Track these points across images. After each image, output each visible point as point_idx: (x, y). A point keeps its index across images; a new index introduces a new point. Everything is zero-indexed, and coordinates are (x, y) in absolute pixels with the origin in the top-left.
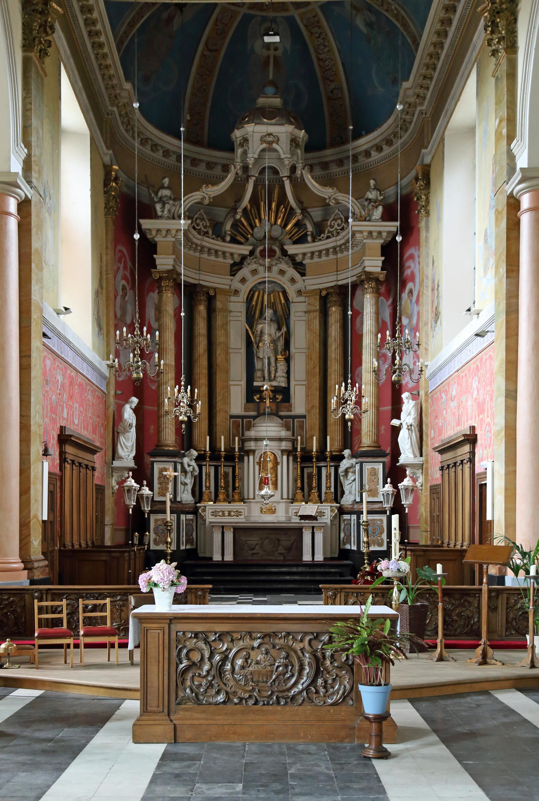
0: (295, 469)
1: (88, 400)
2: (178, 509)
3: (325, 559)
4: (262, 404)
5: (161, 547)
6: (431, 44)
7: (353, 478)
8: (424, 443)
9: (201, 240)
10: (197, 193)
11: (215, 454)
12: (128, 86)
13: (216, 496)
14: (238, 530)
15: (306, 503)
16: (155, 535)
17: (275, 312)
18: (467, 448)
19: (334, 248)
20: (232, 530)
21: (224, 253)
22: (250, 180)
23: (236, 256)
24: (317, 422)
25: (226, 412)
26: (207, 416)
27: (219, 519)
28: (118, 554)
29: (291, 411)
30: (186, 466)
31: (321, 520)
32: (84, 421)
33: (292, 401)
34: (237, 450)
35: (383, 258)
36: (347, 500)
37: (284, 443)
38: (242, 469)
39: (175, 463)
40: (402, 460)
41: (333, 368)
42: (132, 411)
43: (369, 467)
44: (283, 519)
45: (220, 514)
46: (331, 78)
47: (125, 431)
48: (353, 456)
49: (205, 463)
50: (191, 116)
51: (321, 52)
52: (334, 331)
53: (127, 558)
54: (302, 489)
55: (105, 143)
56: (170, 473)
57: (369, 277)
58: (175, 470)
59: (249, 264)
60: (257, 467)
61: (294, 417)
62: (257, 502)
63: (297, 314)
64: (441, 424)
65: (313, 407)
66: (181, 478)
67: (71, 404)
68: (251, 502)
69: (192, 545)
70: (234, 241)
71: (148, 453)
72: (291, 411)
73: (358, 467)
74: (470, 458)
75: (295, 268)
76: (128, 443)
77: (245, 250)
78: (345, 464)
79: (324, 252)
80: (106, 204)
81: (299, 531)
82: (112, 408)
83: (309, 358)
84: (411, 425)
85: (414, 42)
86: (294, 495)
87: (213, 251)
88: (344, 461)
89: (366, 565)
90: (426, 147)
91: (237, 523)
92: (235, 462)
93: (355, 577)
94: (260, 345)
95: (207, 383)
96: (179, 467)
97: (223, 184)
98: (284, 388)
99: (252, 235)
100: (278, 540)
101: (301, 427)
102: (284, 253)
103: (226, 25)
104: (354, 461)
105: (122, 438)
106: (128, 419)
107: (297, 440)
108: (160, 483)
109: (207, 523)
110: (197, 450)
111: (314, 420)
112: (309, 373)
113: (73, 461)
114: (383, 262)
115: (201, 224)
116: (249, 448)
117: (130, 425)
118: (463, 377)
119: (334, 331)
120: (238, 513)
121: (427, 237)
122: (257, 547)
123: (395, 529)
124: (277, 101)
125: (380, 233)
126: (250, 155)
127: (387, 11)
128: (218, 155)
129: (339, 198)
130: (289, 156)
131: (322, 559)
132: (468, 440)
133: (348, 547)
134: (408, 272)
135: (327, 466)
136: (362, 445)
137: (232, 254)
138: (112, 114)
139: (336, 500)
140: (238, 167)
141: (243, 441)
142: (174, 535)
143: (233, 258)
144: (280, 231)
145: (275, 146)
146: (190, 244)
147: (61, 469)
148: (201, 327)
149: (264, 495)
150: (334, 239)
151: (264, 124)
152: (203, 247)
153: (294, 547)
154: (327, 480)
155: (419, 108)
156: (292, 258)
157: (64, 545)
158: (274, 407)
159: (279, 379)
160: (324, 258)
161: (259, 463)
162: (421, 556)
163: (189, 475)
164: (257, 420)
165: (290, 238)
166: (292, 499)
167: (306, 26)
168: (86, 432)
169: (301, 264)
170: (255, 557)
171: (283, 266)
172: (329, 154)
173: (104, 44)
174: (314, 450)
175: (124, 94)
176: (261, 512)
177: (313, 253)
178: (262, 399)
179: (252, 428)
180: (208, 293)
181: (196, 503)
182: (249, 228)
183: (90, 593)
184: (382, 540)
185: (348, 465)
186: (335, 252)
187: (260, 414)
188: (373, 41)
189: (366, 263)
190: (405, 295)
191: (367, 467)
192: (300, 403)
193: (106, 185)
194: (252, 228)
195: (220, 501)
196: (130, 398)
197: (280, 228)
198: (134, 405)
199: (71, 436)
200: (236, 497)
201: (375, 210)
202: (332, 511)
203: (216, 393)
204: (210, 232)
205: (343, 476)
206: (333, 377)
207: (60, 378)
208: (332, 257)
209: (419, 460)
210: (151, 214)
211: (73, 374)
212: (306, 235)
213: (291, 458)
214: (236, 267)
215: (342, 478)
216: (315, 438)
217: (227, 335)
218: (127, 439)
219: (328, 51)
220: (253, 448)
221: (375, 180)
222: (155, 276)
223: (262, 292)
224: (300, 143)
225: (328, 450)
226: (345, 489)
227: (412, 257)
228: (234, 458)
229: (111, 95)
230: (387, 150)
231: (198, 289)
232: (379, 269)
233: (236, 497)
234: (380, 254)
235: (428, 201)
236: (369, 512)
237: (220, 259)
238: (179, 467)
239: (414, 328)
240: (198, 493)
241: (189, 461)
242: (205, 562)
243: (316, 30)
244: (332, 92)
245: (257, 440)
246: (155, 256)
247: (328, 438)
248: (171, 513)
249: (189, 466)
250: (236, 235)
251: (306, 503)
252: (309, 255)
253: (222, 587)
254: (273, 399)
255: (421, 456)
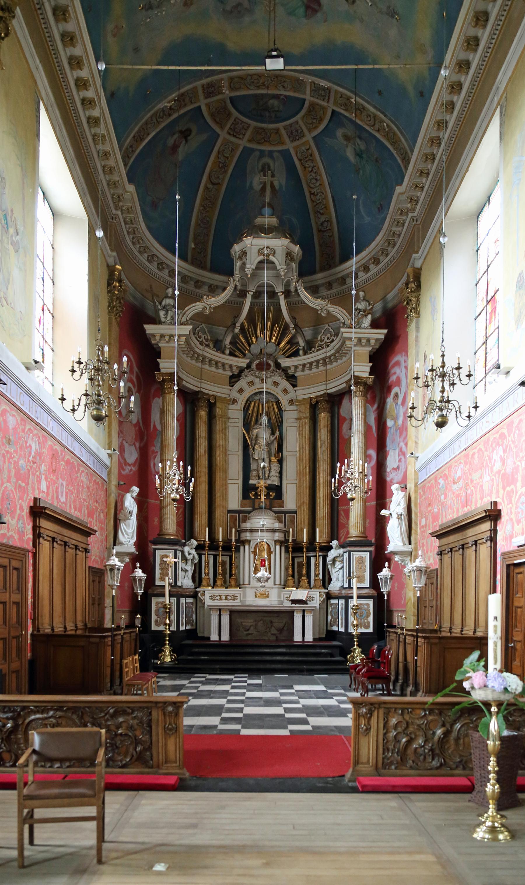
0: (287, 558)
1: (82, 481)
2: (177, 592)
3: (315, 639)
4: (257, 500)
5: (162, 628)
6: (435, 123)
7: (340, 566)
8: (413, 532)
9: (202, 350)
10: (198, 303)
11: (213, 545)
12: (131, 188)
13: (215, 581)
14: (234, 613)
15: (297, 589)
16: (156, 617)
17: (269, 420)
18: (486, 526)
19: (324, 359)
20: (228, 613)
21: (224, 365)
22: (248, 295)
23: (234, 368)
24: (307, 517)
25: (224, 507)
26: (207, 511)
27: (217, 603)
28: (97, 640)
29: (283, 507)
30: (187, 554)
31: (310, 604)
32: (74, 501)
33: (284, 498)
34: (233, 541)
35: (371, 364)
36: (335, 586)
37: (277, 534)
38: (238, 558)
39: (176, 550)
40: (390, 548)
41: (322, 468)
42: (132, 500)
43: (357, 556)
44: (275, 603)
45: (218, 598)
46: (322, 211)
47: (126, 519)
48: (342, 546)
49: (204, 552)
50: (195, 244)
51: (312, 186)
52: (323, 436)
53: (110, 643)
54: (293, 576)
55: (110, 245)
56: (171, 559)
57: (358, 381)
58: (176, 557)
59: (246, 376)
60: (252, 556)
61: (285, 513)
62: (252, 588)
63: (289, 421)
64: (436, 510)
65: (303, 503)
66: (181, 565)
67: (54, 478)
68: (246, 587)
69: (192, 625)
70: (232, 354)
71: (150, 541)
72: (283, 507)
73: (346, 556)
74: (491, 537)
75: (288, 380)
76: (129, 529)
77: (243, 362)
78: (332, 554)
79: (314, 364)
80: (109, 303)
81: (291, 614)
82: (113, 498)
83: (300, 459)
84: (401, 515)
85: (403, 159)
86: (286, 581)
87: (214, 363)
88: (332, 551)
89: (355, 647)
90: (417, 252)
91: (233, 606)
92: (231, 551)
93: (345, 657)
94: (256, 447)
95: (207, 481)
96: (179, 554)
97: (223, 295)
98: (277, 486)
99: (249, 351)
100: (271, 622)
101: (292, 521)
102: (278, 365)
103: (227, 158)
104: (341, 551)
105: (123, 526)
106: (128, 507)
107: (288, 532)
108: (161, 569)
109: (206, 606)
110: (197, 541)
111: (303, 516)
112: (299, 473)
113: (53, 540)
114: (371, 368)
115: (203, 337)
116: (245, 539)
117: (131, 513)
118: (474, 454)
119: (323, 436)
120: (234, 598)
121: (417, 337)
122: (252, 628)
123: (496, 618)
124: (274, 221)
125: (368, 340)
126: (248, 266)
127: (378, 131)
128: (218, 278)
129: (330, 309)
130: (285, 267)
131: (311, 640)
132: (489, 516)
133: (335, 628)
134: (393, 378)
135: (316, 556)
136: (350, 536)
137: (231, 366)
138: (116, 218)
139: (324, 586)
140: (237, 279)
141: (239, 532)
142: (174, 617)
143: (231, 370)
144: (275, 348)
145: (272, 258)
146: (192, 352)
147: (34, 545)
148: (202, 431)
149: (261, 578)
150: (324, 350)
151: (261, 237)
152: (204, 358)
153: (285, 629)
154: (316, 568)
155: (410, 215)
156: (285, 370)
157: (38, 628)
158: (268, 503)
159: (272, 478)
160: (314, 370)
161: (254, 553)
162: (435, 644)
163: (189, 563)
164: (252, 514)
165: (283, 354)
166: (284, 585)
167: (300, 160)
168: (79, 514)
169: (293, 377)
170: (249, 637)
171: (277, 379)
172: (319, 277)
173: (99, 119)
174: (305, 541)
175: (127, 196)
176: (256, 596)
177: (304, 365)
178: (257, 495)
179: (248, 521)
180: (209, 401)
181: (196, 588)
182: (246, 345)
183: (9, 707)
184: (369, 623)
185: (335, 555)
186: (325, 364)
187: (256, 508)
188: (361, 172)
189: (356, 369)
190: (390, 400)
191: (355, 556)
192: (290, 500)
193: (109, 284)
194: (250, 346)
195: (218, 586)
196: (131, 487)
197: (274, 345)
198: (135, 494)
199: (45, 508)
200: (233, 583)
201: (364, 318)
202: (320, 596)
203: (215, 490)
204: (211, 345)
205: (331, 564)
206: (322, 475)
207: (35, 447)
208: (321, 368)
209: (408, 548)
210: (156, 321)
211: (58, 447)
212: (298, 350)
213: (283, 548)
214: (234, 379)
215: (329, 566)
216: (305, 530)
217: (226, 439)
218: (128, 526)
219: (320, 185)
220: (248, 538)
221: (363, 291)
222: (159, 379)
223: (257, 402)
224: (295, 258)
225: (318, 541)
226: (332, 577)
227: (398, 364)
228: (231, 548)
229: (113, 195)
230: (374, 269)
231: (199, 396)
232: (367, 375)
233: (233, 583)
234: (368, 361)
235: (418, 303)
236: (359, 597)
237: (221, 371)
238: (179, 554)
239: (399, 428)
240: (197, 578)
241: (190, 550)
242: (202, 642)
243: (309, 163)
244: (322, 224)
245: (252, 531)
246: (158, 360)
247: (317, 530)
248: (170, 597)
249: (189, 554)
250: (235, 351)
251: (297, 589)
252: (301, 367)
253: (218, 666)
254: (267, 495)
255: (410, 544)
